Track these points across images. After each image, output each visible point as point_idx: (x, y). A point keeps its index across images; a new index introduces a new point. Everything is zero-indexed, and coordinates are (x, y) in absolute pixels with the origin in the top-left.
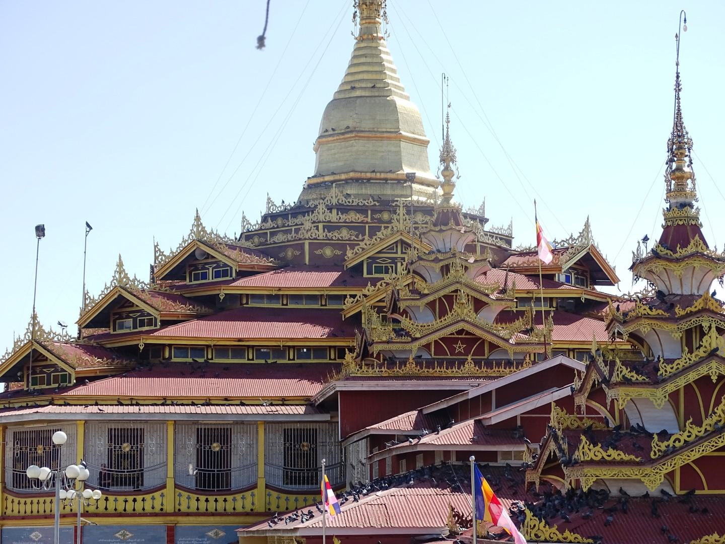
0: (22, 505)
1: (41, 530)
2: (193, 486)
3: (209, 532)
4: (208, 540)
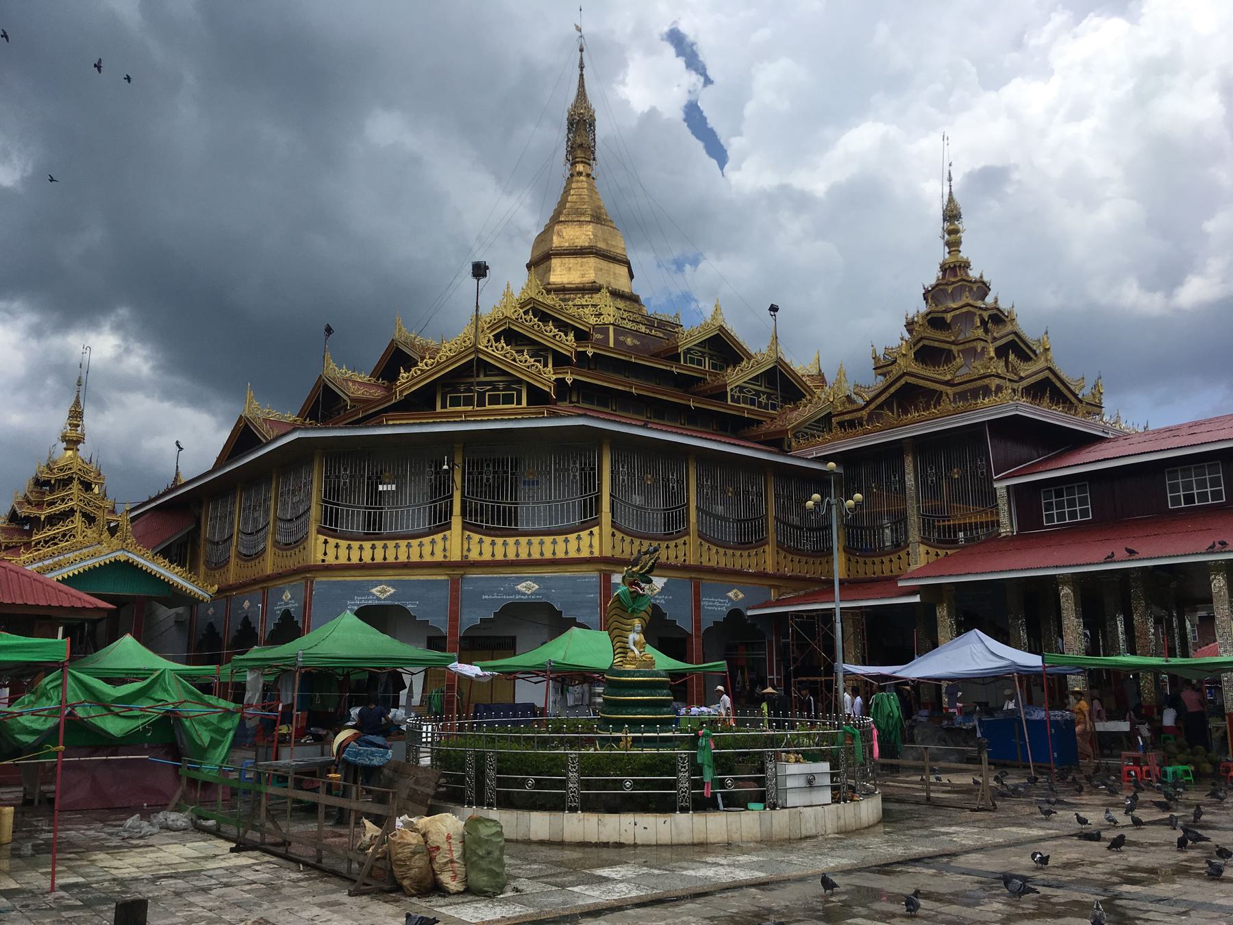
1: (535, 580)
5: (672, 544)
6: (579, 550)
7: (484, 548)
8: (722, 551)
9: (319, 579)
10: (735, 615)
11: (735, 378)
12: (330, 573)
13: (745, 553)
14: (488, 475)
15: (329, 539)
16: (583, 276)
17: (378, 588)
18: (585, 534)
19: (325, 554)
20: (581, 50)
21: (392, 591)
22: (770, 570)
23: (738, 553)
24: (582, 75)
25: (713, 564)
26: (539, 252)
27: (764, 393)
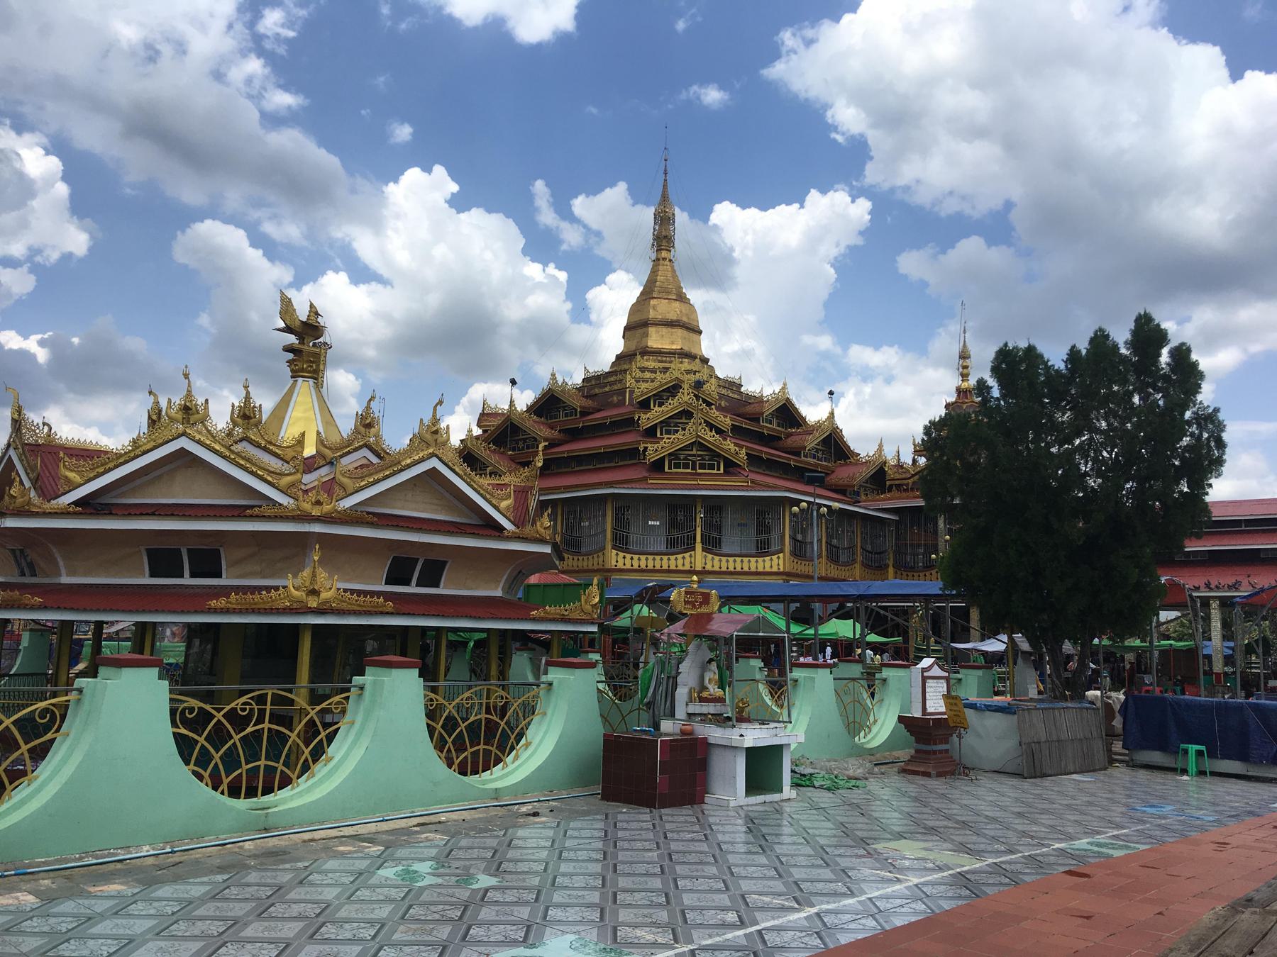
7: (714, 563)
14: (681, 517)
24: (665, 186)
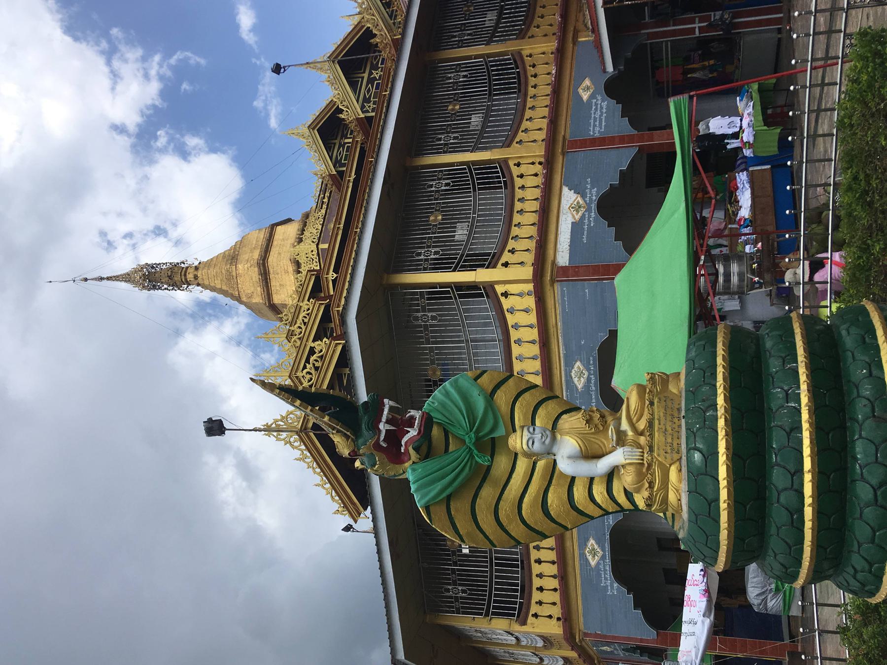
0: (523, 169)
1: (569, 365)
2: (502, 193)
3: (581, 98)
4: (596, 98)
5: (518, 182)
6: (526, 311)
8: (528, 114)
9: (582, 627)
10: (612, 88)
11: (352, 112)
12: (574, 617)
13: (532, 81)
15: (532, 612)
16: (287, 272)
17: (590, 558)
18: (506, 303)
19: (550, 617)
20: (86, 280)
21: (592, 541)
22: (553, 45)
23: (531, 91)
24: (108, 279)
25: (544, 123)
26: (270, 314)
27: (371, 73)
